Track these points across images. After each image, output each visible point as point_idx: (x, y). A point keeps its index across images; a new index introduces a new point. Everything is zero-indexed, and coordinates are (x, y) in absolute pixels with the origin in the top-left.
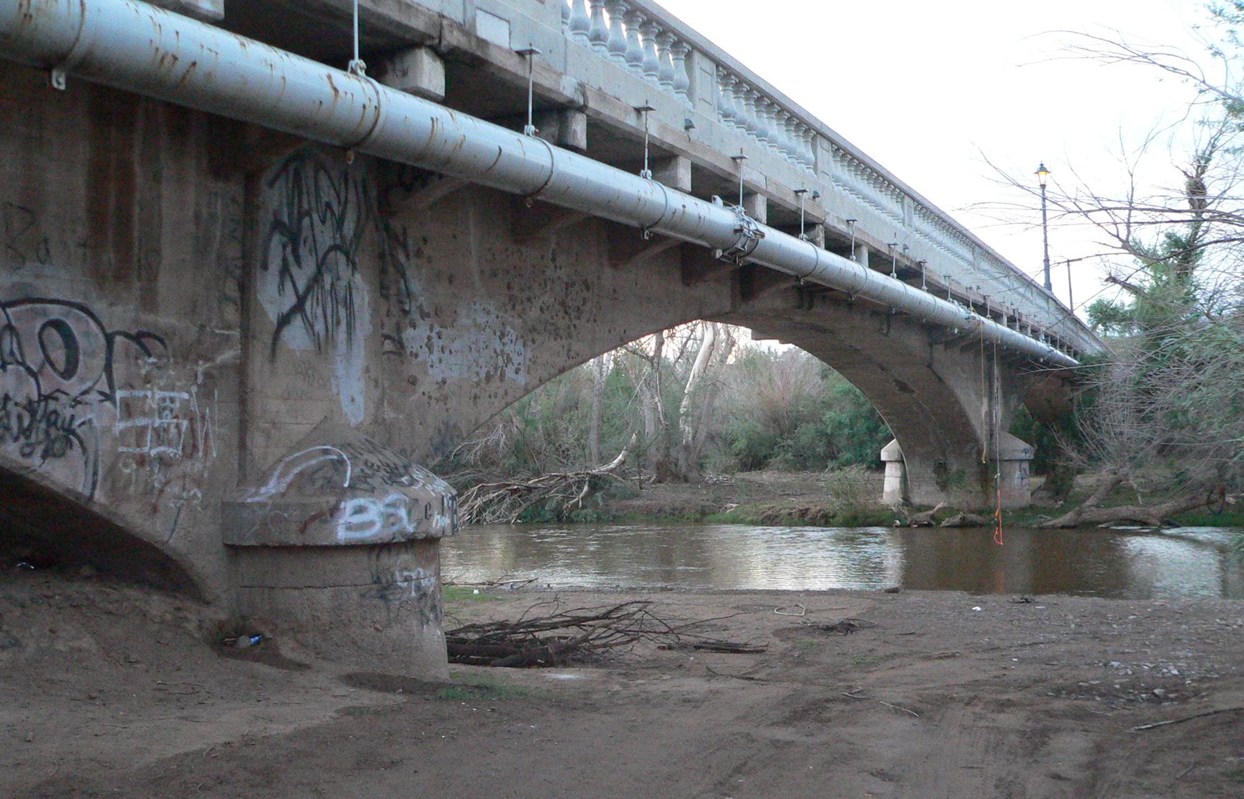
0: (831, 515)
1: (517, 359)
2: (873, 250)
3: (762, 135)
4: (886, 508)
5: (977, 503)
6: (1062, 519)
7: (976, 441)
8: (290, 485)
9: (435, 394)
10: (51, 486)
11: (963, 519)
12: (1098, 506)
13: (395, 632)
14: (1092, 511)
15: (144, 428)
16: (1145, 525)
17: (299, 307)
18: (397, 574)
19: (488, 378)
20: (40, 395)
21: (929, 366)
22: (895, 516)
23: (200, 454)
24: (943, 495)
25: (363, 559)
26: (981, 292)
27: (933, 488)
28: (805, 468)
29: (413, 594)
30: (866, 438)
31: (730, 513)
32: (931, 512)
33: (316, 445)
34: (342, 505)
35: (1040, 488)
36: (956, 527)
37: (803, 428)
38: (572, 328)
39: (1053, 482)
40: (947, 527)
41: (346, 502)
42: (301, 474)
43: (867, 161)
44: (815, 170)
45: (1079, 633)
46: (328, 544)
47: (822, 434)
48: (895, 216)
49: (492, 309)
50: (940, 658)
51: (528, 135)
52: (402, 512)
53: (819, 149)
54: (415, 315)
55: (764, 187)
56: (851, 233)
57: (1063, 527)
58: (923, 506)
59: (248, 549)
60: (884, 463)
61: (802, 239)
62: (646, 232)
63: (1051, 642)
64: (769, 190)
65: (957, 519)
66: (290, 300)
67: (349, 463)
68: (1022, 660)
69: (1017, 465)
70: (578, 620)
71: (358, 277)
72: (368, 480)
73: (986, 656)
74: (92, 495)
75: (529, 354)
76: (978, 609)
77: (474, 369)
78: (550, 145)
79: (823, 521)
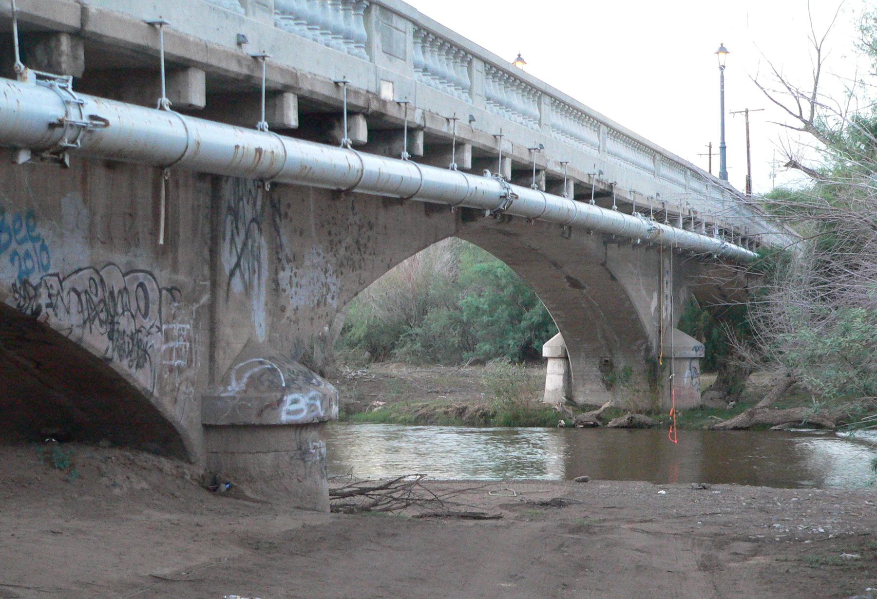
1: (333, 288)
2: (577, 182)
3: (508, 107)
4: (549, 407)
5: (645, 404)
6: (733, 421)
7: (646, 338)
8: (247, 385)
9: (293, 318)
10: (137, 386)
11: (631, 419)
12: (770, 407)
13: (308, 483)
15: (172, 349)
16: (818, 427)
17: (238, 265)
18: (310, 444)
19: (318, 304)
20: (136, 330)
21: (603, 265)
22: (559, 416)
23: (194, 365)
24: (608, 394)
25: (291, 434)
26: (660, 198)
27: (599, 386)
28: (435, 361)
29: (318, 458)
30: (508, 327)
31: (380, 411)
32: (597, 412)
33: (252, 358)
34: (285, 398)
35: (711, 388)
36: (623, 427)
37: (431, 315)
38: (362, 261)
39: (725, 382)
40: (616, 427)
41: (287, 396)
42: (251, 377)
43: (577, 105)
44: (540, 124)
45: (749, 508)
46: (275, 423)
47: (458, 321)
48: (592, 145)
49: (320, 251)
50: (641, 522)
51: (404, 159)
52: (318, 403)
53: (543, 106)
54: (284, 262)
55: (511, 153)
56: (564, 173)
57: (735, 428)
58: (587, 405)
59: (224, 427)
61: (533, 189)
62: (453, 207)
63: (727, 513)
64: (514, 154)
65: (624, 419)
66: (234, 260)
67: (279, 370)
68: (704, 524)
69: (687, 363)
70: (365, 490)
71: (263, 238)
72: (295, 381)
73: (676, 520)
74: (153, 391)
75: (339, 285)
76: (663, 492)
77: (312, 298)
78: (416, 164)
79: (482, 420)
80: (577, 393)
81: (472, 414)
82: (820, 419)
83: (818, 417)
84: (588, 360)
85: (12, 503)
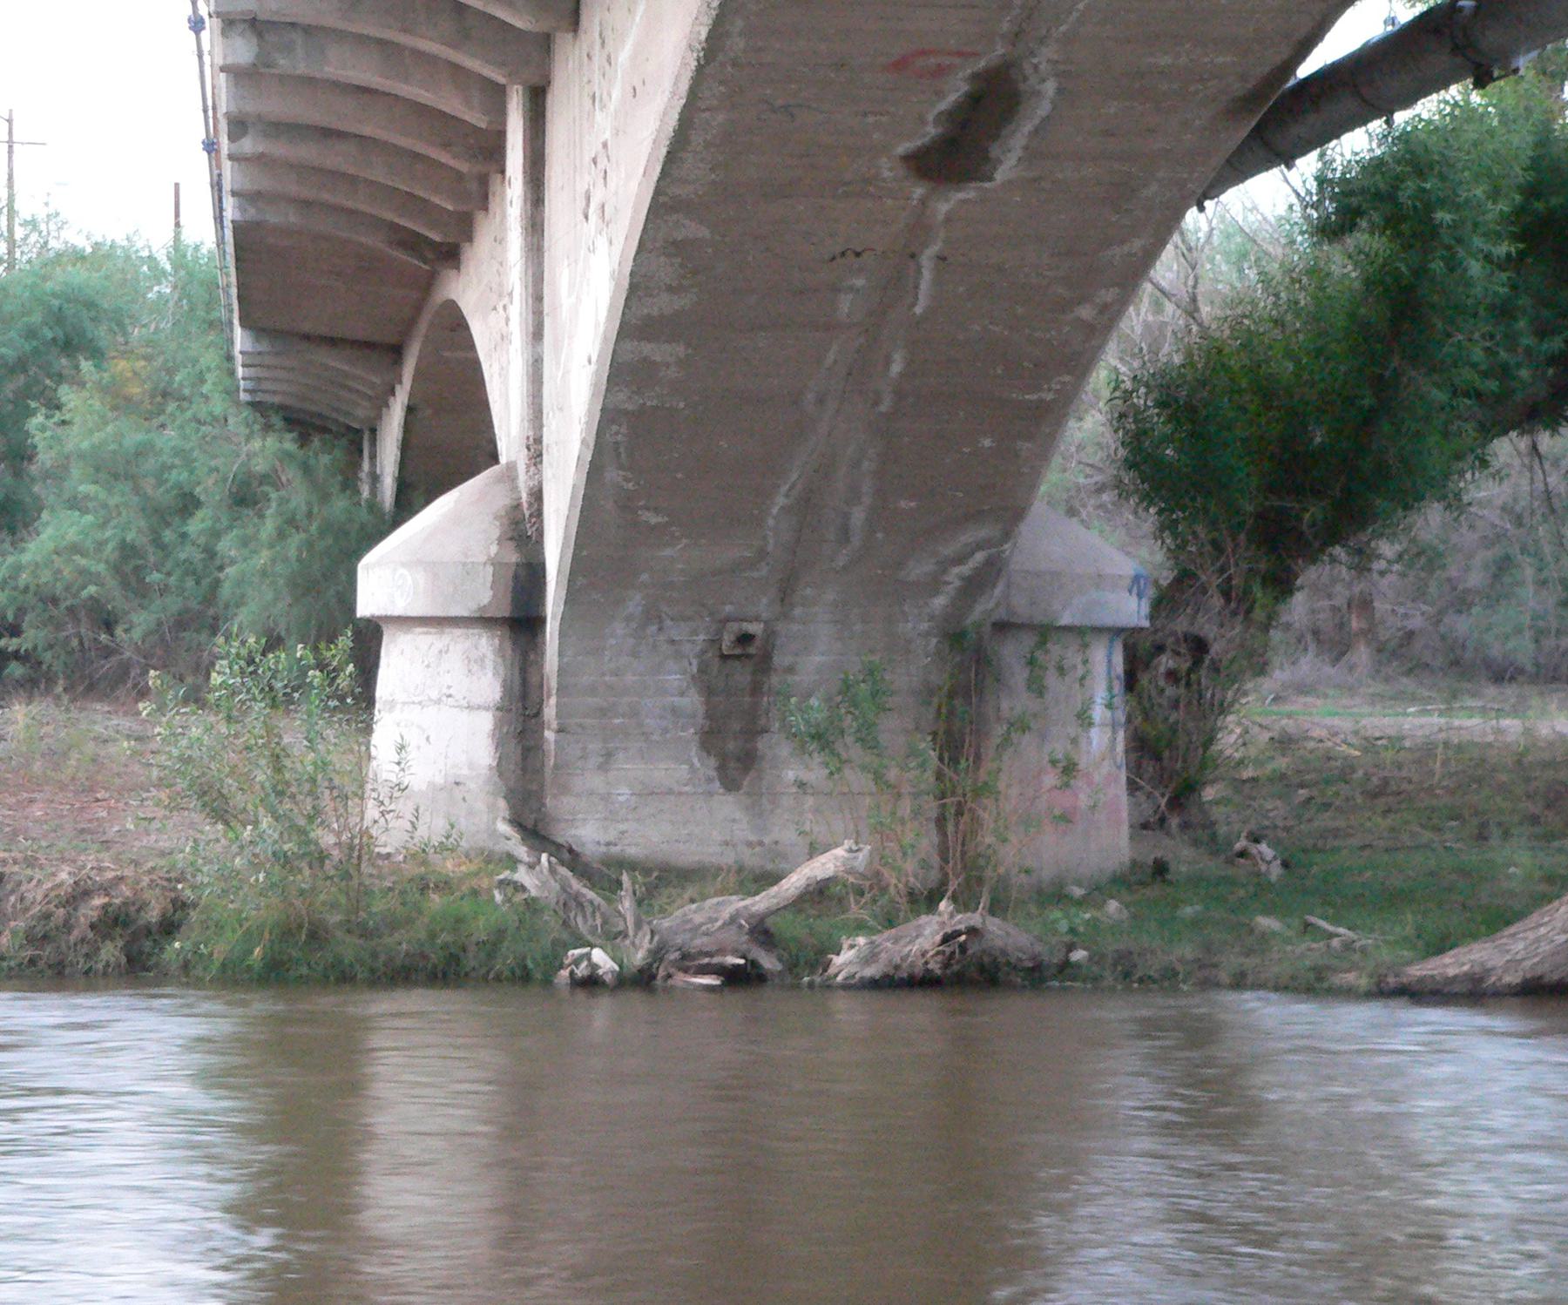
0: (153, 915)
32: (761, 902)
40: (874, 985)
46: (1267, 70)
60: (369, 637)
79: (110, 952)
81: (47, 916)
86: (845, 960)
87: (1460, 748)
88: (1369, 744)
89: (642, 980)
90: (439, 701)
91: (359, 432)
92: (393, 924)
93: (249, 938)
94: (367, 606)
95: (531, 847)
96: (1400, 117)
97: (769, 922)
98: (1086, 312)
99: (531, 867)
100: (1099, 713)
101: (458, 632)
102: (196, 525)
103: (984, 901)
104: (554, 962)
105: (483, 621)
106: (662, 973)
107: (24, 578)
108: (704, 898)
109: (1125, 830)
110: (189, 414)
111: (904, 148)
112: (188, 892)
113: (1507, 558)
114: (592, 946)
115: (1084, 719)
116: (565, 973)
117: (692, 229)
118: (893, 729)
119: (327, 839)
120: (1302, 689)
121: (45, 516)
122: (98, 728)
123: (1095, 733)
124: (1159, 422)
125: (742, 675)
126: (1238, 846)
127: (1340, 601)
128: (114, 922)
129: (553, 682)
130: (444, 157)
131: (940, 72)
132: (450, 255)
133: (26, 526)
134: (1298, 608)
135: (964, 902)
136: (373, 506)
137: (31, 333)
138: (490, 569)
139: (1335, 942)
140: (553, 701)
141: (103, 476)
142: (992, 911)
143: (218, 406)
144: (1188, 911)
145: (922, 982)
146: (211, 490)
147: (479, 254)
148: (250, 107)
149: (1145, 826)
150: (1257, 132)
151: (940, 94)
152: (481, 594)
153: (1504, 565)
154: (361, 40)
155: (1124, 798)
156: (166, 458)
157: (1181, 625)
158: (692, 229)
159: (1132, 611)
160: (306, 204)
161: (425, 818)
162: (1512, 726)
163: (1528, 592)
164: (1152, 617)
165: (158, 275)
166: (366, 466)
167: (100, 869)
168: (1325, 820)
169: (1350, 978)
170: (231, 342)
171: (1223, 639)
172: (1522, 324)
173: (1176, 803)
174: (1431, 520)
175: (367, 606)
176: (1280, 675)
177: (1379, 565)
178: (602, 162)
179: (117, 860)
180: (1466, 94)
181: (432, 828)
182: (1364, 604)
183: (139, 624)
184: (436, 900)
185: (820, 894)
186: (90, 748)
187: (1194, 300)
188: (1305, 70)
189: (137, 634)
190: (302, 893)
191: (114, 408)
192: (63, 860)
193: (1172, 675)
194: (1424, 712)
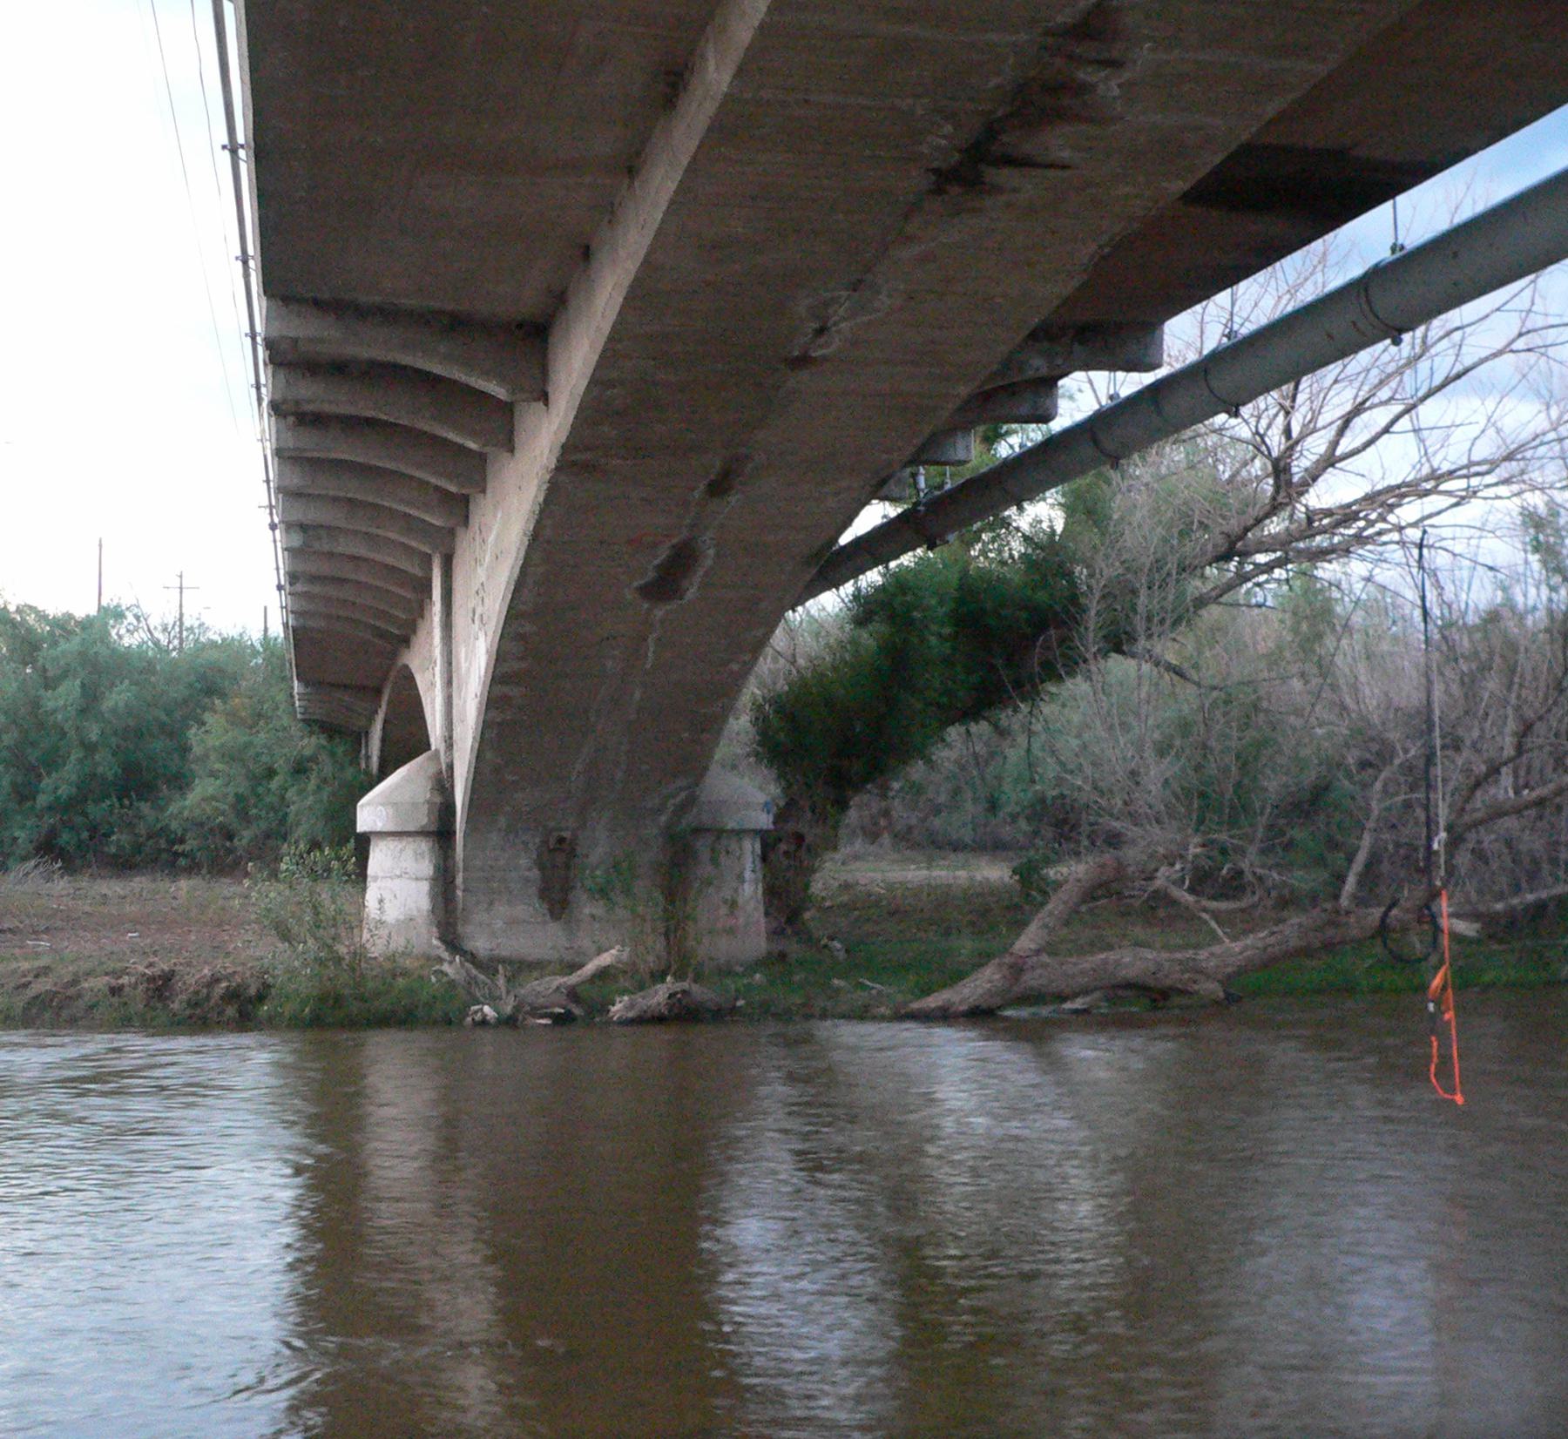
0: (252, 991)
14: (1045, 966)
24: (554, 928)
27: (528, 908)
32: (573, 979)
60: (363, 843)
79: (231, 1011)
80: (469, 929)
81: (197, 993)
82: (1187, 976)
83: (1183, 972)
84: (511, 837)
85: (1101, 247)
86: (618, 1009)
87: (937, 886)
88: (890, 887)
89: (509, 1022)
90: (400, 877)
91: (360, 734)
92: (378, 994)
93: (304, 1003)
94: (361, 827)
95: (451, 954)
96: (893, 564)
97: (579, 990)
98: (735, 667)
99: (451, 963)
100: (748, 875)
101: (411, 839)
102: (274, 784)
103: (691, 975)
104: (464, 1012)
105: (422, 833)
106: (520, 1018)
107: (186, 813)
108: (542, 976)
109: (764, 934)
110: (271, 726)
111: (636, 584)
112: (270, 979)
113: (959, 787)
114: (483, 1004)
115: (740, 878)
116: (469, 1019)
117: (528, 628)
118: (640, 887)
119: (342, 950)
120: (856, 857)
121: (197, 781)
122: (226, 892)
123: (746, 886)
124: (775, 720)
125: (560, 859)
126: (822, 943)
127: (874, 811)
128: (233, 995)
129: (461, 865)
130: (401, 592)
131: (655, 545)
132: (405, 641)
133: (187, 785)
134: (853, 816)
135: (680, 977)
136: (367, 772)
137: (191, 685)
138: (426, 806)
139: (874, 992)
140: (461, 874)
141: (226, 759)
142: (695, 981)
143: (285, 722)
144: (797, 978)
145: (658, 1019)
146: (280, 764)
147: (419, 640)
148: (301, 567)
149: (774, 933)
150: (820, 572)
151: (655, 557)
152: (422, 819)
153: (957, 792)
154: (355, 533)
155: (763, 920)
156: (258, 750)
157: (791, 827)
158: (528, 628)
159: (765, 821)
160: (328, 617)
161: (394, 937)
162: (962, 874)
163: (969, 806)
164: (774, 823)
165: (255, 653)
166: (363, 752)
167: (225, 968)
168: (868, 927)
169: (882, 1010)
170: (292, 688)
171: (812, 834)
172: (959, 668)
173: (790, 921)
174: (917, 770)
175: (361, 827)
176: (844, 851)
177: (891, 794)
178: (481, 593)
179: (233, 963)
180: (925, 553)
181: (398, 943)
182: (886, 813)
183: (246, 836)
184: (401, 981)
185: (603, 974)
186: (220, 902)
187: (794, 656)
188: (845, 539)
189: (245, 841)
190: (330, 979)
191: (232, 724)
192: (205, 962)
193: (786, 853)
194: (919, 869)
